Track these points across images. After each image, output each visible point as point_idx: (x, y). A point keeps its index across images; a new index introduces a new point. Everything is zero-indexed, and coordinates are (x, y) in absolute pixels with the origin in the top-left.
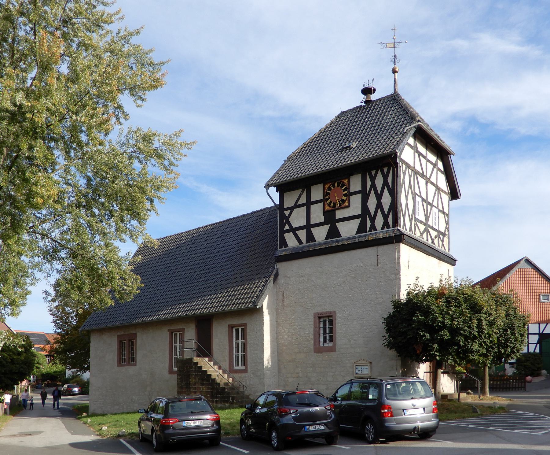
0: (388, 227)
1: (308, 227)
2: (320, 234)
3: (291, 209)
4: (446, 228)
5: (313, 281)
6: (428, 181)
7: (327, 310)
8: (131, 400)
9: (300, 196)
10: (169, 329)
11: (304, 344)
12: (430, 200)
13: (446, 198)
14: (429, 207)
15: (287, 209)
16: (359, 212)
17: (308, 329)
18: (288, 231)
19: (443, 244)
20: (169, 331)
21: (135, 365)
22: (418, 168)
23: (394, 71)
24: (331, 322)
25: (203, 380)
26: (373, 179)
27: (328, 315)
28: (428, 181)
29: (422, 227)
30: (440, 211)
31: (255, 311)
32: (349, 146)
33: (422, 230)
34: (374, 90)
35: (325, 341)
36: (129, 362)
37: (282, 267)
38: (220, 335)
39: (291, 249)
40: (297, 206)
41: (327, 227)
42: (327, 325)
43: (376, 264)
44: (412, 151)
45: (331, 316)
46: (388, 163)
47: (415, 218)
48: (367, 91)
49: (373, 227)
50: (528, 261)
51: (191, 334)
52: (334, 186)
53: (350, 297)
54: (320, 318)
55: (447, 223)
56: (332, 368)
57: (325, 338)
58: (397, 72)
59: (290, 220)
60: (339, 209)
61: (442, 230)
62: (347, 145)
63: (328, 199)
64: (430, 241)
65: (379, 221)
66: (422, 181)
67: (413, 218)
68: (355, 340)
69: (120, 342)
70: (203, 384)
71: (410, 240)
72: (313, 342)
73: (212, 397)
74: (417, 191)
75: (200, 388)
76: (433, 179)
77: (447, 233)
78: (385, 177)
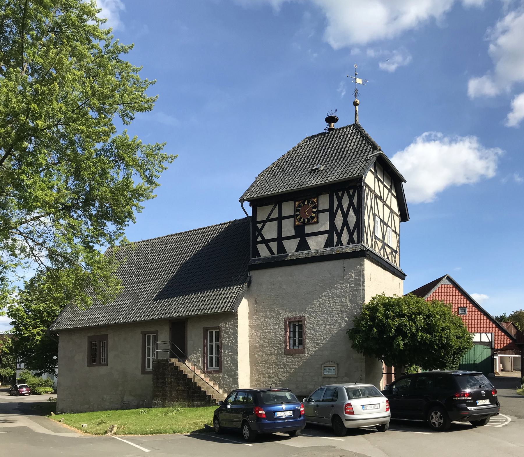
1: (280, 239)
2: (291, 246)
3: (264, 222)
4: (398, 246)
5: (284, 289)
6: (385, 204)
8: (102, 399)
9: (272, 211)
12: (386, 221)
13: (397, 219)
14: (385, 227)
15: (260, 222)
16: (327, 228)
17: (280, 333)
18: (260, 242)
19: (395, 261)
20: (142, 333)
21: (107, 365)
22: (377, 192)
24: (301, 327)
25: (179, 380)
26: (340, 200)
28: (385, 204)
29: (380, 244)
30: (393, 231)
31: (231, 315)
32: (318, 169)
33: (380, 247)
34: (337, 120)
35: (294, 344)
36: (100, 363)
37: (255, 275)
38: (194, 337)
40: (269, 220)
41: (298, 240)
42: (297, 329)
43: (343, 275)
44: (373, 177)
45: (301, 321)
46: (356, 185)
47: (375, 236)
48: (331, 120)
49: (340, 243)
50: (449, 278)
51: (164, 336)
52: (304, 204)
54: (290, 323)
55: (398, 242)
57: (294, 341)
58: (358, 105)
59: (262, 232)
60: (308, 224)
61: (395, 247)
62: (315, 168)
63: (298, 215)
64: (386, 257)
65: (345, 237)
66: (380, 204)
67: (374, 236)
69: (90, 343)
71: (372, 255)
74: (377, 213)
76: (388, 203)
77: (398, 250)
78: (351, 198)
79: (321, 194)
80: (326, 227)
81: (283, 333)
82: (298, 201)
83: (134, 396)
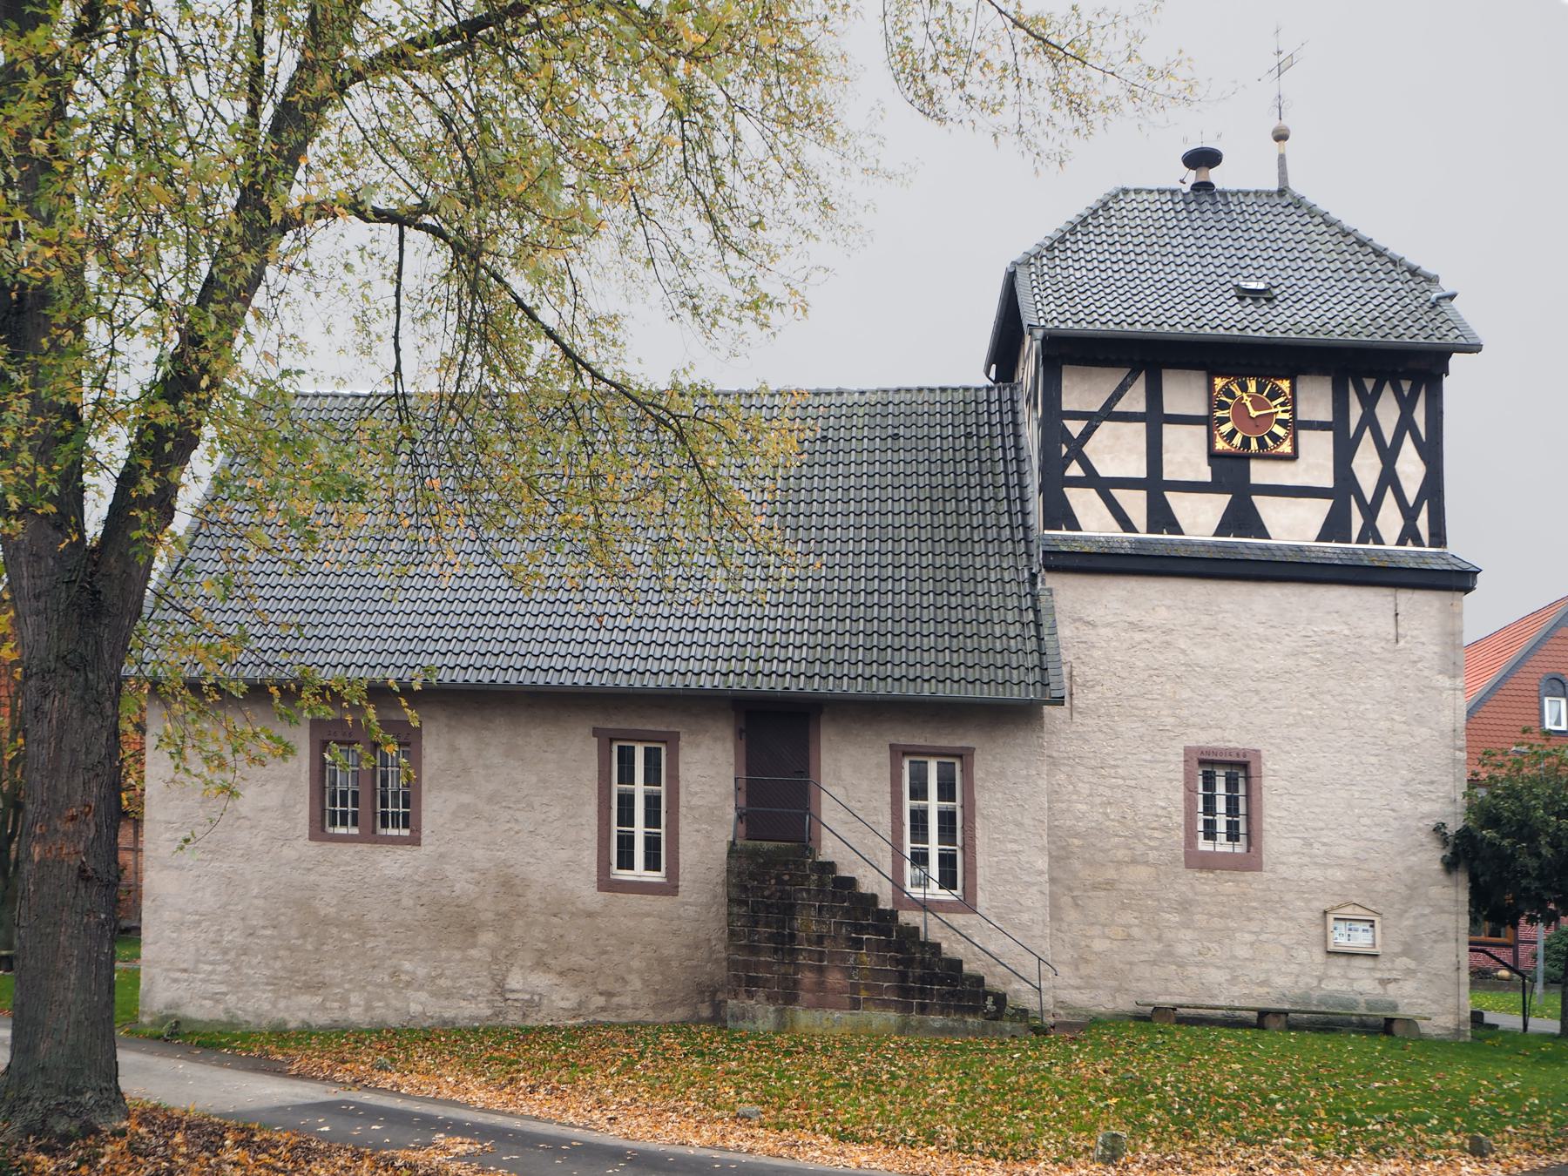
0: (1418, 541)
2: (1200, 518)
7: (1231, 745)
10: (600, 725)
11: (1150, 838)
21: (415, 841)
23: (1281, 136)
25: (861, 929)
26: (1369, 403)
27: (1234, 758)
39: (1087, 540)
40: (1108, 413)
43: (1392, 637)
48: (1203, 158)
49: (1371, 532)
53: (1311, 717)
56: (1249, 919)
59: (1087, 449)
65: (1390, 520)
68: (1324, 844)
70: (857, 944)
72: (1182, 834)
73: (904, 992)
75: (844, 958)
78: (1407, 406)
79: (1305, 371)
80: (1325, 478)
81: (1179, 796)
82: (1222, 376)
83: (561, 974)
